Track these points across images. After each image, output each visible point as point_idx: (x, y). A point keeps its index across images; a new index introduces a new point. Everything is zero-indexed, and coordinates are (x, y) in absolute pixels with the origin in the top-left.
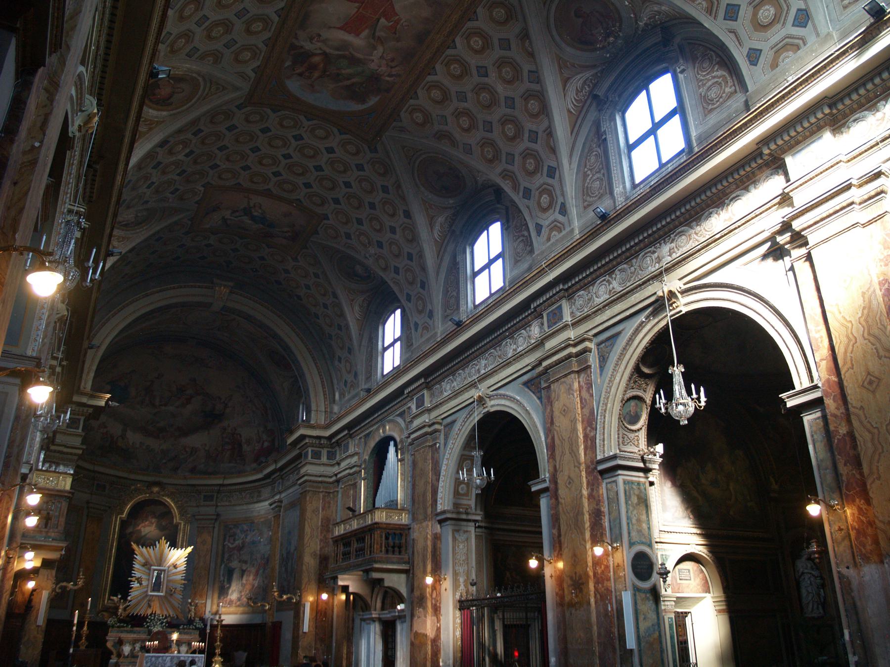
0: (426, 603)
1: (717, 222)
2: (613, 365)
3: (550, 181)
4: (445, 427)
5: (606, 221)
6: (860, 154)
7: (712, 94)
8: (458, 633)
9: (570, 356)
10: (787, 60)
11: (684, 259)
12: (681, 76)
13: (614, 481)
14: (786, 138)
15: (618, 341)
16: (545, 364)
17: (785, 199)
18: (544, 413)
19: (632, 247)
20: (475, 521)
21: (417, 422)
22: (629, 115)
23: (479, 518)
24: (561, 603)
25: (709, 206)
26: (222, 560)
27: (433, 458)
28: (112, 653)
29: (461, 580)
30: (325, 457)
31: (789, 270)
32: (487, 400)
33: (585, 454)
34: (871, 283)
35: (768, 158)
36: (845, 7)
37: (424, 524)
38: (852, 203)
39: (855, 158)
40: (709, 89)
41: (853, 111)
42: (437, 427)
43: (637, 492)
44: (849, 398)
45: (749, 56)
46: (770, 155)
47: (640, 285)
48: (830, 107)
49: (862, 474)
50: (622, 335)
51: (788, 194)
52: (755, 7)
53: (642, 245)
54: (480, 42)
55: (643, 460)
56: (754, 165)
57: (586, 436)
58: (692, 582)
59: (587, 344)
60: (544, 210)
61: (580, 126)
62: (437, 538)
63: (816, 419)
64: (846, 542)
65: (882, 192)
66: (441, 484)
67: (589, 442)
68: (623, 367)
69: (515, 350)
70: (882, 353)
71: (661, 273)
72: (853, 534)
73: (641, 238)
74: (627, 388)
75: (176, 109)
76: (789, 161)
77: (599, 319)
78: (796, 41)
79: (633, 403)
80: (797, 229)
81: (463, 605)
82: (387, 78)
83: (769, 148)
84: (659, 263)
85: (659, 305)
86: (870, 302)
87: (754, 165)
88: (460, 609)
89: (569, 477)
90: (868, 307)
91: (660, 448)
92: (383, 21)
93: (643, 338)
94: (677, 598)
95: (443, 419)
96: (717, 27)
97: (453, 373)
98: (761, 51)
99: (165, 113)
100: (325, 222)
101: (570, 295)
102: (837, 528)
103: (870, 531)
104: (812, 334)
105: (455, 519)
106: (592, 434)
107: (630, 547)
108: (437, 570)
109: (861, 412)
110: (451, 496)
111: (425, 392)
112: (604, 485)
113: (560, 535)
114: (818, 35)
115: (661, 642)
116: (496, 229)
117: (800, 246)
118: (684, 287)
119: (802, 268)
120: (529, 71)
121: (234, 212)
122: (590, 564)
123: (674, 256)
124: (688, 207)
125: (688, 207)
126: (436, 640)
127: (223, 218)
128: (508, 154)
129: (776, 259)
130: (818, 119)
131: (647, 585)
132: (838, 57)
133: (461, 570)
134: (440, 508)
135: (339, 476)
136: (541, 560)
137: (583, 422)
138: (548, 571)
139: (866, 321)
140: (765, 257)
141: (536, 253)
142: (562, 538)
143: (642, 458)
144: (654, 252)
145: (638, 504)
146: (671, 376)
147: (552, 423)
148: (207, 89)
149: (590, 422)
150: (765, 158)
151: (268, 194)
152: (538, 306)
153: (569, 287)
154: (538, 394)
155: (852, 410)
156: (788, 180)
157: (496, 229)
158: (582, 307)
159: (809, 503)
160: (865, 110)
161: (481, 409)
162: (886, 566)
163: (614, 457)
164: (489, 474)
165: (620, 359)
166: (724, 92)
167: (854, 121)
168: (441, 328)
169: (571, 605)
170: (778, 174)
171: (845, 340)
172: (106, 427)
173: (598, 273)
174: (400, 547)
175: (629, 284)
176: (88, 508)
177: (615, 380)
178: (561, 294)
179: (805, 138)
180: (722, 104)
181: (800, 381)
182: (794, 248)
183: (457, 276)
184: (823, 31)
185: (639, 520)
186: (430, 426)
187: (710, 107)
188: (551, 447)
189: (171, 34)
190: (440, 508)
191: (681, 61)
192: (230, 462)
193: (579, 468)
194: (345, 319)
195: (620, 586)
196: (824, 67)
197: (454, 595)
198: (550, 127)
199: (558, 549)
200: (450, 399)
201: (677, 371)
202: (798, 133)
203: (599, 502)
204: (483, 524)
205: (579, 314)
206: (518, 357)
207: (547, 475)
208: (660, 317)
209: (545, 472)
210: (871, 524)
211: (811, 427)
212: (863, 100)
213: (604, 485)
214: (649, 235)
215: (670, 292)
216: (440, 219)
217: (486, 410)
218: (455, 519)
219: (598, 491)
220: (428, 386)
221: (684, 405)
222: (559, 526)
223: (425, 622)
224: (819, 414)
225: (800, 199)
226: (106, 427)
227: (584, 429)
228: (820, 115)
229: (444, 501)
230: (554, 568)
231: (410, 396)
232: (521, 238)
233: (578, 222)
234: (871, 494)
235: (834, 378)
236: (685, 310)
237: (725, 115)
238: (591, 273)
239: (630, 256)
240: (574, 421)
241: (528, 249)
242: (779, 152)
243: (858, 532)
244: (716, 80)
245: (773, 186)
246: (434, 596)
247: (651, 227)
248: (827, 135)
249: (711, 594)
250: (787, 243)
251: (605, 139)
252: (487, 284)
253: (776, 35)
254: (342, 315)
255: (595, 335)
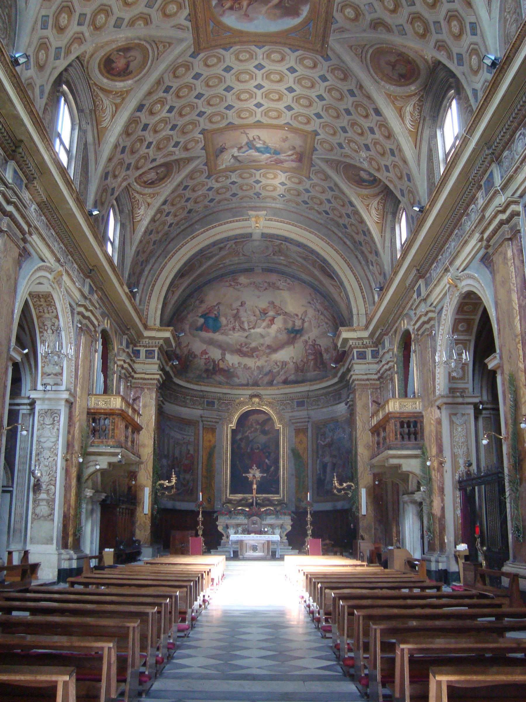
26: (317, 457)
28: (223, 535)
30: (370, 357)
75: (139, 73)
99: (130, 82)
100: (318, 137)
121: (241, 148)
127: (233, 156)
135: (381, 372)
148: (156, 50)
151: (259, 125)
172: (207, 353)
174: (415, 434)
176: (202, 421)
189: (85, 15)
192: (314, 371)
194: (366, 225)
197: (453, 476)
204: (489, 406)
216: (408, 109)
226: (207, 353)
254: (362, 221)
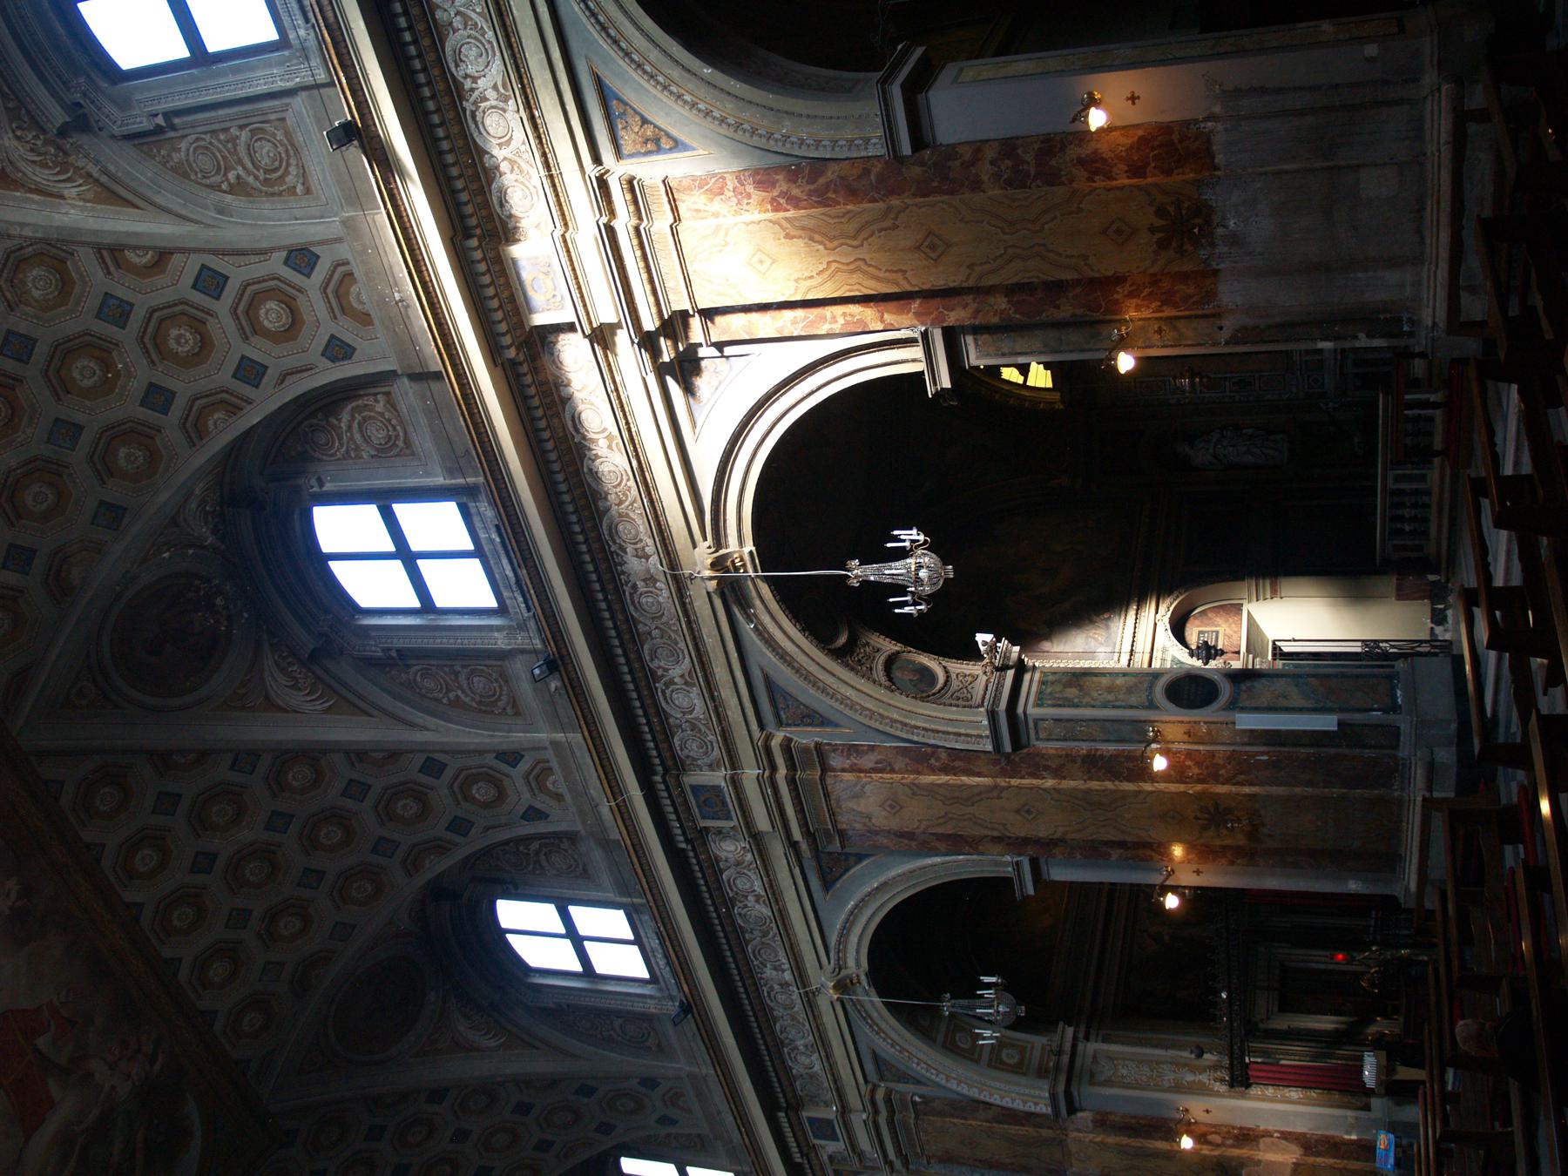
0: (1231, 1159)
1: (611, 461)
2: (823, 697)
3: (448, 774)
4: (882, 1079)
5: (558, 662)
6: (560, 205)
7: (377, 434)
8: (1295, 1094)
9: (791, 781)
10: (364, 297)
11: (661, 532)
12: (328, 487)
13: (1036, 724)
14: (499, 315)
15: (781, 682)
16: (797, 835)
17: (602, 337)
18: (889, 852)
19: (616, 627)
20: (1075, 1038)
21: (864, 1142)
22: (364, 601)
23: (1070, 1031)
24: (1246, 855)
25: (578, 472)
27: (941, 1114)
29: (1190, 1078)
31: (721, 351)
32: (843, 973)
33: (979, 775)
34: (774, 223)
35: (525, 353)
36: (308, 191)
37: (1073, 1147)
38: (637, 229)
39: (563, 214)
40: (367, 440)
41: (487, 204)
42: (880, 1095)
43: (1058, 688)
44: (952, 285)
45: (334, 359)
46: (518, 349)
47: (689, 623)
48: (470, 237)
49: (1077, 282)
50: (771, 673)
51: (593, 330)
52: (255, 332)
53: (617, 607)
54: (147, 852)
55: (1003, 668)
56: (528, 379)
57: (945, 770)
58: (1221, 630)
59: (775, 743)
60: (501, 795)
61: (360, 697)
62: (1103, 1122)
63: (977, 345)
64: (1181, 324)
65: (630, 182)
66: (996, 1099)
67: (957, 763)
68: (830, 680)
69: (758, 897)
70: (888, 223)
71: (676, 578)
72: (1168, 312)
73: (603, 605)
74: (868, 675)
76: (539, 319)
77: (734, 714)
78: (337, 276)
79: (897, 674)
80: (658, 324)
81: (1240, 1080)
82: (157, 1067)
83: (508, 347)
84: (656, 581)
85: (731, 590)
86: (803, 228)
87: (528, 379)
88: (1248, 1086)
89: (1017, 812)
90: (812, 234)
91: (982, 638)
92: (42, 1042)
93: (785, 633)
94: (1248, 651)
95: (866, 1081)
96: (267, 401)
97: (779, 1044)
98: (332, 336)
101: (677, 766)
102: (1157, 336)
103: (1166, 285)
104: (837, 328)
105: (1069, 1077)
106: (944, 755)
107: (1157, 708)
108: (1169, 1129)
109: (978, 269)
110: (1023, 1080)
111: (805, 1114)
112: (1040, 744)
113: (1122, 844)
114: (339, 240)
115: (1328, 676)
116: (510, 912)
117: (686, 326)
118: (710, 541)
119: (728, 326)
120: (232, 768)
122: (1182, 788)
123: (650, 549)
124: (570, 508)
125: (570, 508)
126: (1308, 1144)
128: (374, 850)
129: (697, 371)
130: (484, 258)
131: (1226, 689)
132: (396, 207)
133: (1170, 1077)
134: (1044, 1108)
136: (1164, 889)
137: (919, 773)
138: (1187, 878)
139: (832, 239)
140: (689, 390)
141: (580, 828)
142: (1129, 839)
143: (997, 669)
144: (635, 587)
145: (1081, 688)
146: (865, 583)
147: (910, 836)
149: (921, 756)
150: (521, 357)
152: (684, 833)
153: (663, 763)
154: (852, 859)
155: (971, 283)
156: (570, 327)
157: (510, 912)
158: (703, 744)
159: (1115, 369)
160: (490, 186)
161: (859, 990)
162: (1222, 266)
163: (992, 715)
164: (989, 986)
165: (814, 682)
166: (382, 414)
167: (502, 206)
168: (683, 1062)
169: (1253, 834)
170: (555, 343)
171: (856, 277)
173: (648, 702)
175: (682, 645)
177: (854, 696)
178: (671, 781)
179: (508, 285)
180: (401, 422)
181: (908, 361)
182: (687, 337)
183: (584, 1005)
184: (337, 230)
185: (1110, 689)
186: (876, 1112)
187: (401, 444)
188: (956, 843)
190: (1044, 1108)
191: (301, 481)
193: (1004, 789)
195: (1226, 734)
196: (404, 230)
197: (1218, 1095)
198: (347, 753)
199: (1149, 852)
200: (828, 1057)
201: (858, 572)
202: (496, 295)
203: (1070, 757)
205: (716, 752)
206: (773, 894)
207: (1008, 858)
208: (754, 594)
209: (997, 863)
210: (1155, 280)
211: (988, 355)
212: (474, 186)
213: (1040, 744)
214: (603, 590)
215: (713, 566)
216: (461, 1029)
217: (863, 978)
218: (1069, 1077)
219: (1050, 757)
220: (795, 1106)
221: (919, 567)
222: (1106, 843)
223: (1270, 1164)
224: (970, 339)
225: (606, 310)
227: (933, 771)
228: (478, 255)
229: (1033, 1097)
230: (1181, 873)
231: (808, 1151)
232: (542, 857)
233: (541, 735)
234: (1109, 273)
235: (916, 305)
236: (749, 547)
237: (423, 420)
238: (646, 715)
239: (631, 633)
240: (916, 789)
241: (565, 844)
242: (519, 332)
243: (1166, 302)
244: (355, 425)
245: (574, 355)
246: (1217, 1139)
247: (589, 582)
248: (516, 251)
249: (1245, 602)
250: (676, 347)
251: (398, 651)
252: (610, 943)
253: (315, 305)
255: (762, 727)
